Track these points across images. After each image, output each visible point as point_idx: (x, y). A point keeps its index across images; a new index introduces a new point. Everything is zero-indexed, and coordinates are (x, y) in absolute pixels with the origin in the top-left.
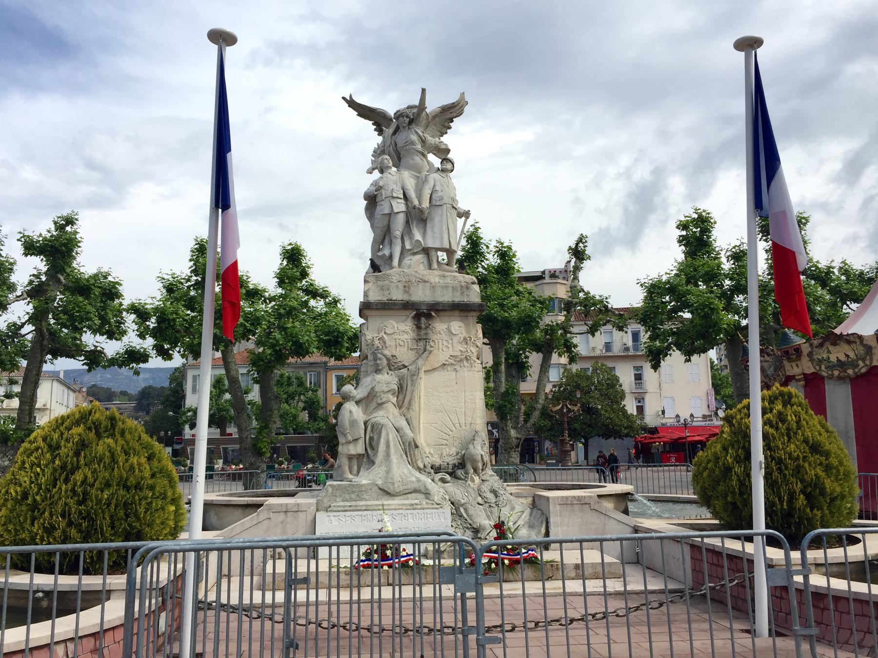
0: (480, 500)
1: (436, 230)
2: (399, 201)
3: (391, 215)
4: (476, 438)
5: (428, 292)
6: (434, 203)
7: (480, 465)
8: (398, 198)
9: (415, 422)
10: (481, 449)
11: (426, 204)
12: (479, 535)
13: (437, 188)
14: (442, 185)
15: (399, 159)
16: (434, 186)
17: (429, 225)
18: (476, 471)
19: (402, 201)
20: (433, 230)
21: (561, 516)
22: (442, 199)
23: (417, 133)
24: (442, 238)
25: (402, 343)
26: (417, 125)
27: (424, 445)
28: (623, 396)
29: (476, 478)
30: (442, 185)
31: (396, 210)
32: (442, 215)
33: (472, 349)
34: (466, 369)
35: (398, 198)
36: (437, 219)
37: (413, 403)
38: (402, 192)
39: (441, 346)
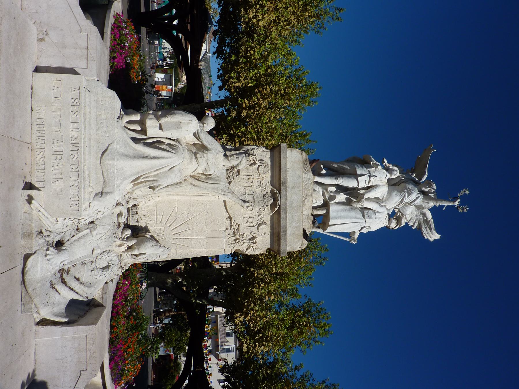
0: (97, 252)
1: (344, 214)
2: (367, 182)
3: (356, 176)
4: (162, 248)
5: (295, 204)
6: (366, 211)
7: (136, 252)
8: (370, 180)
9: (178, 190)
10: (151, 253)
11: (367, 204)
12: (51, 249)
13: (377, 214)
14: (380, 218)
15: (394, 185)
16: (379, 212)
17: (348, 207)
18: (130, 248)
19: (367, 185)
20: (346, 210)
21: (74, 338)
22: (370, 217)
23: (418, 198)
24: (338, 218)
25: (251, 181)
26: (424, 198)
27: (158, 199)
28: (218, 22)
29: (123, 248)
30: (380, 218)
31: (360, 178)
32: (356, 218)
33: (245, 244)
34: (227, 239)
35: (370, 180)
36: (353, 214)
37: (196, 189)
38: (374, 185)
39: (248, 216)
